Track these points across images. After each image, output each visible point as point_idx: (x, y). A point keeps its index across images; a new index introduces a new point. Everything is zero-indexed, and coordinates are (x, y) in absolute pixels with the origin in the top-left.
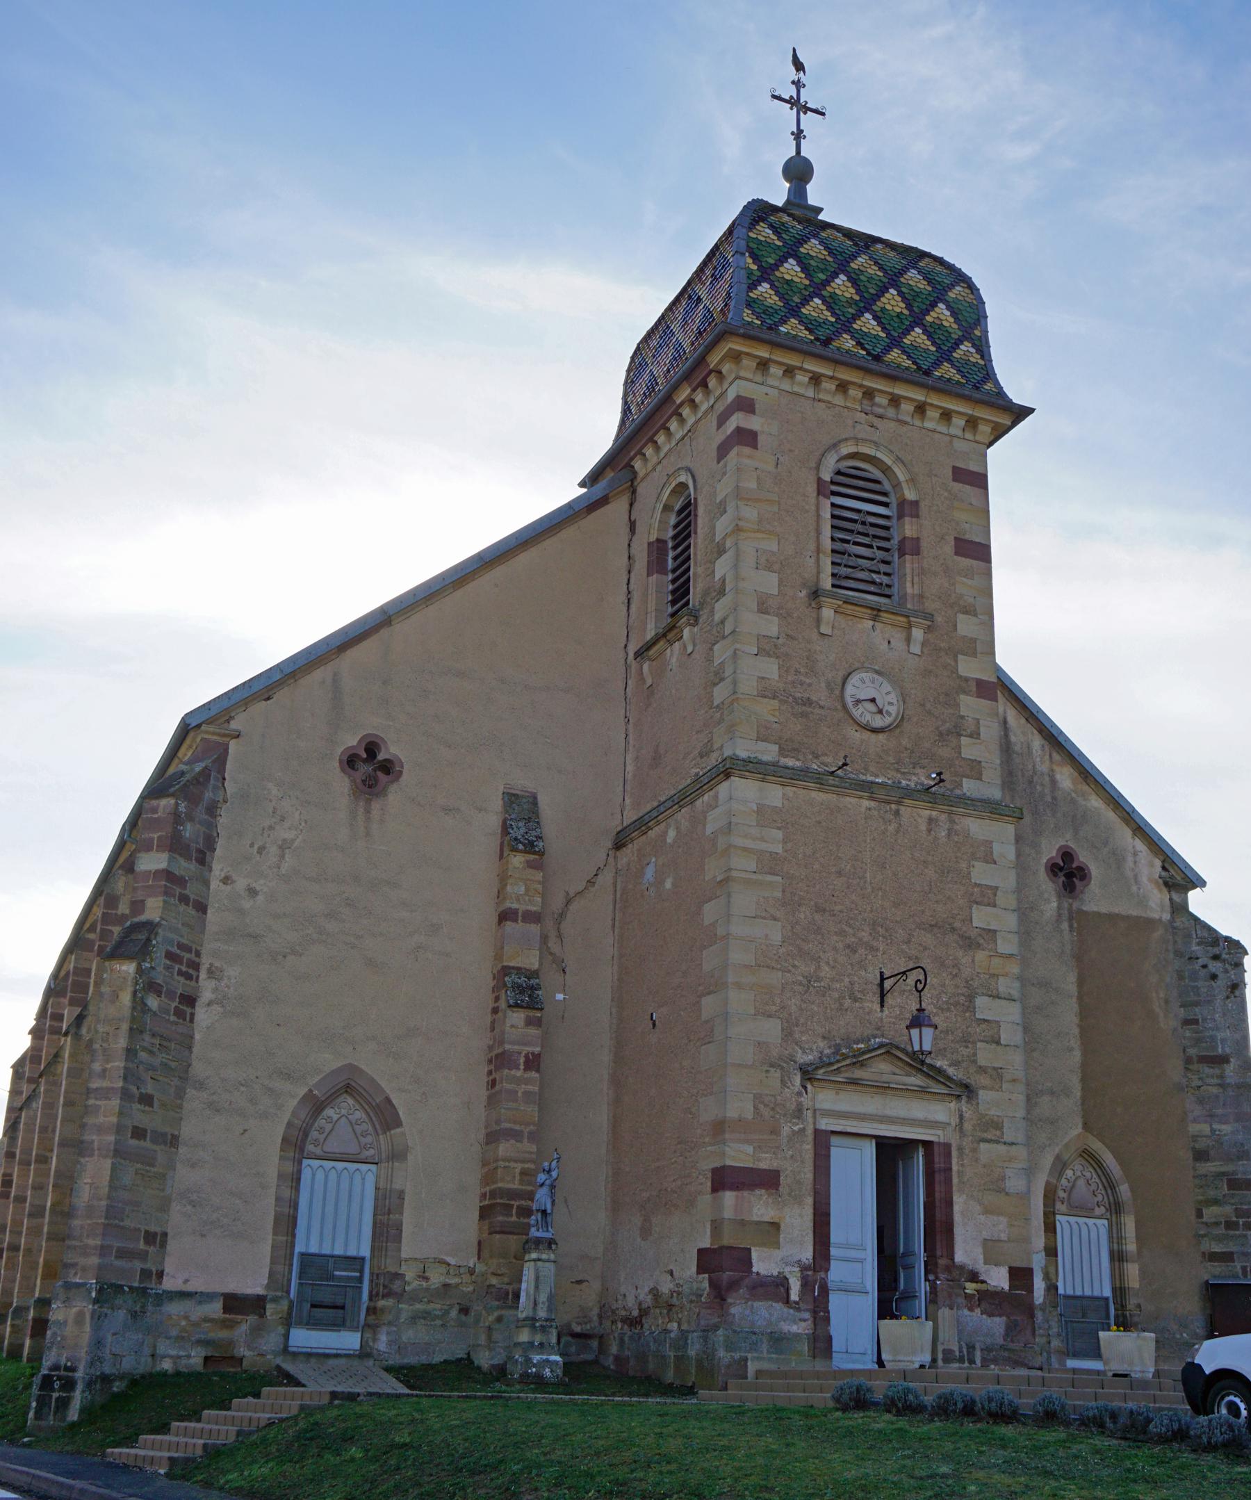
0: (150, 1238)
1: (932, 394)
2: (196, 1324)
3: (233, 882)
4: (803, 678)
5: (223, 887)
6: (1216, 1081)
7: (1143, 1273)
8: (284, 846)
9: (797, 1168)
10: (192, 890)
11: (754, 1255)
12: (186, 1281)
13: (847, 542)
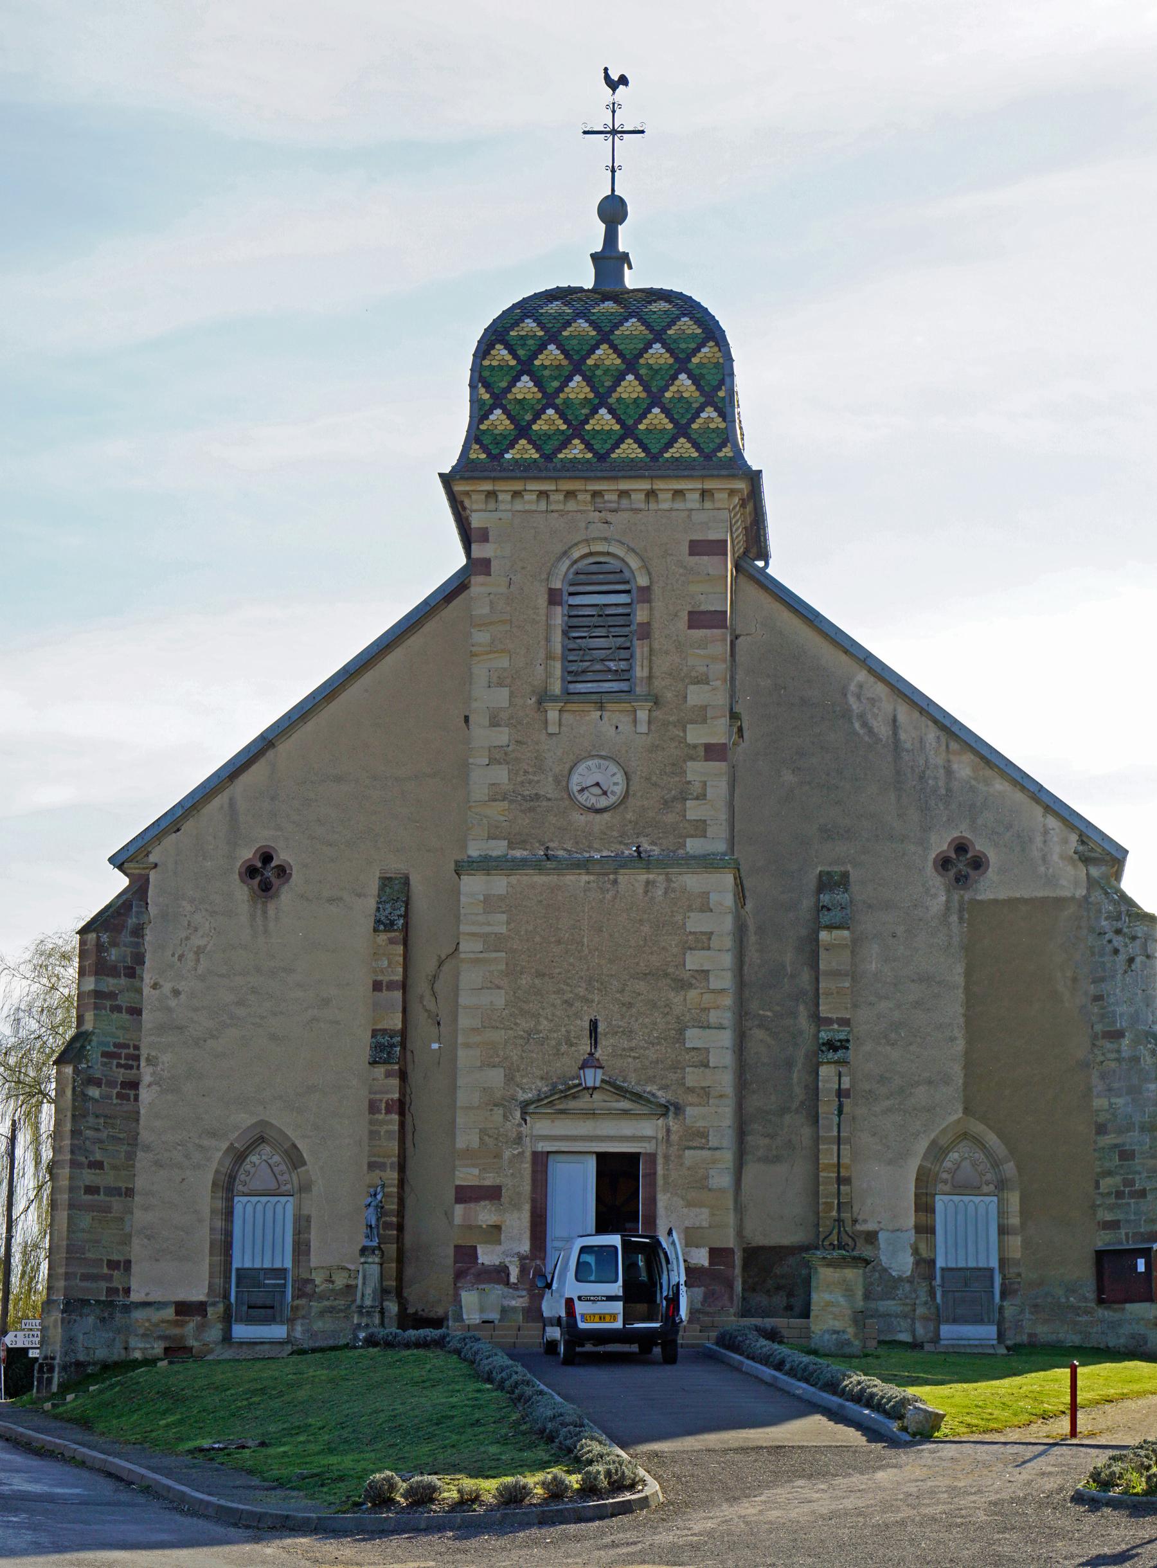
0: (113, 1265)
1: (655, 481)
2: (156, 1325)
3: (161, 987)
4: (531, 777)
5: (153, 992)
6: (1114, 1056)
7: (1026, 1244)
8: (199, 951)
10: (122, 1001)
11: (479, 1251)
12: (147, 1294)
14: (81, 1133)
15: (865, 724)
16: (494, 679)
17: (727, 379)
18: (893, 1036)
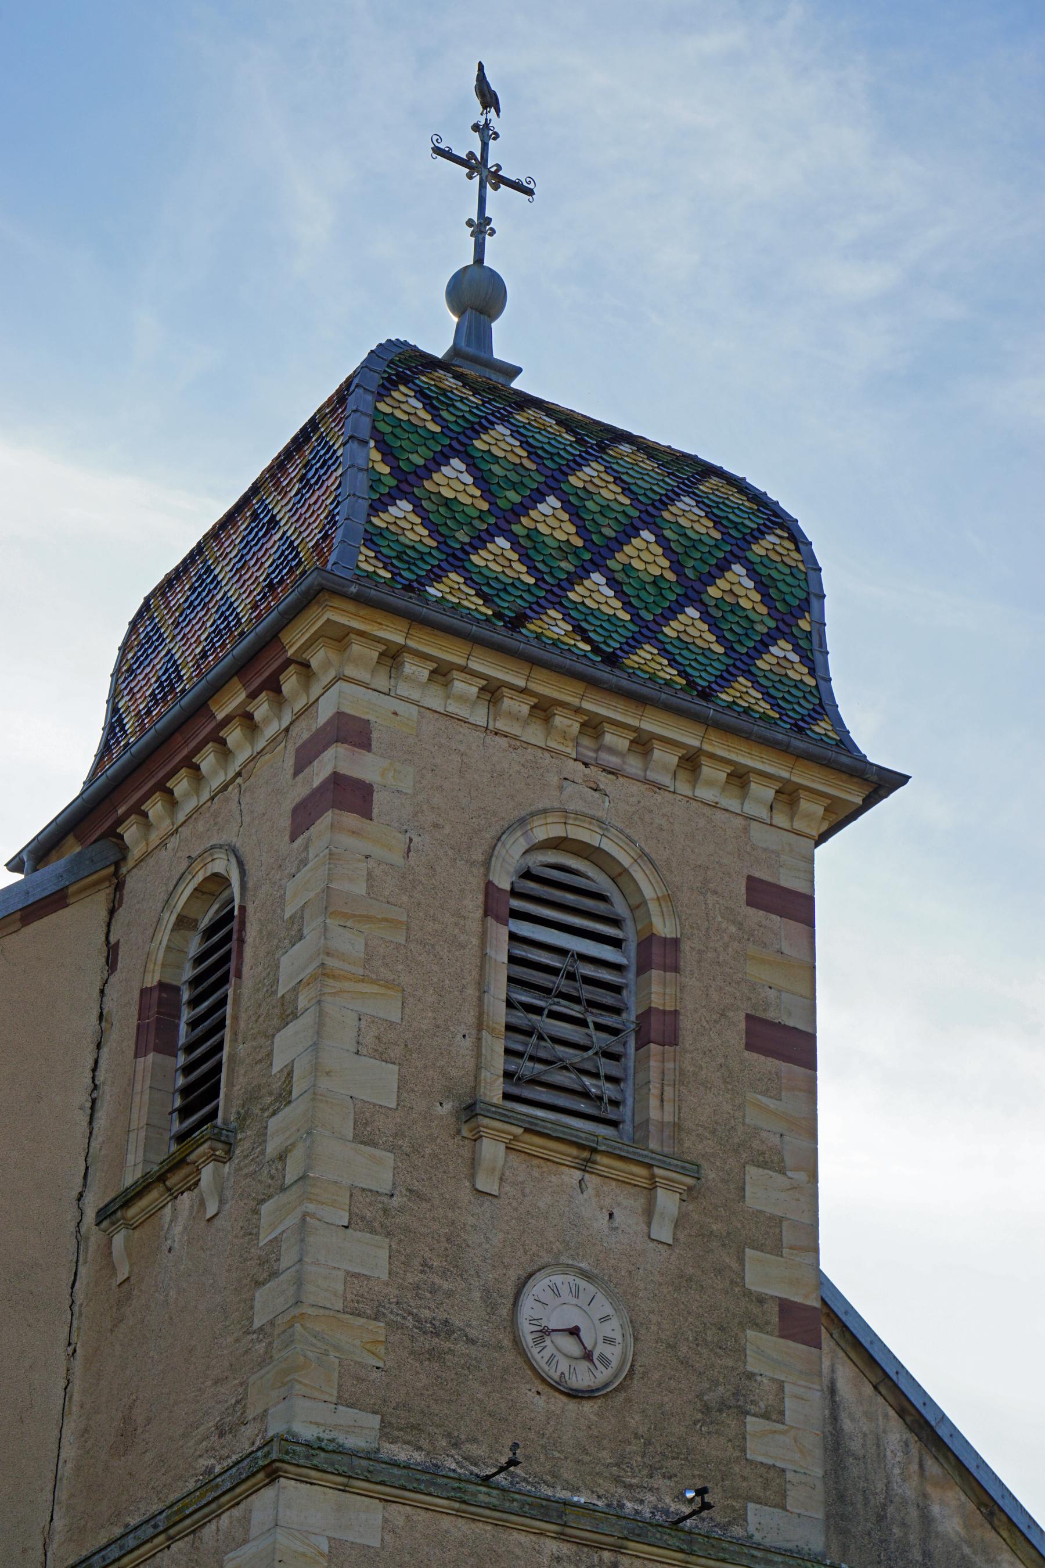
16: (369, 1039)
17: (814, 602)
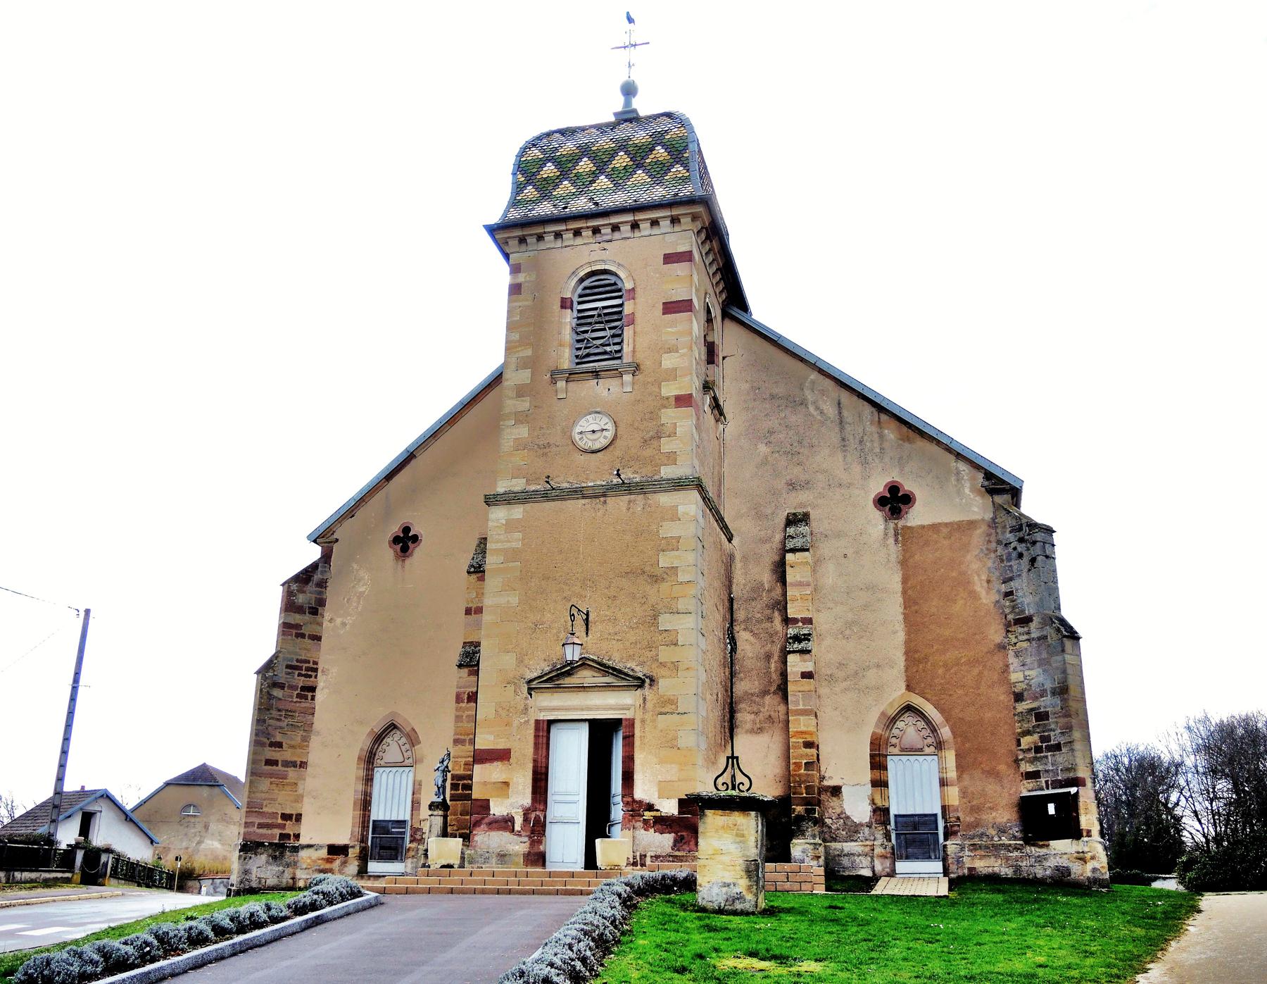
0: (286, 817)
2: (314, 861)
6: (1025, 637)
7: (964, 793)
9: (524, 749)
11: (492, 804)
13: (586, 332)
14: (264, 721)
15: (817, 408)
18: (848, 632)
